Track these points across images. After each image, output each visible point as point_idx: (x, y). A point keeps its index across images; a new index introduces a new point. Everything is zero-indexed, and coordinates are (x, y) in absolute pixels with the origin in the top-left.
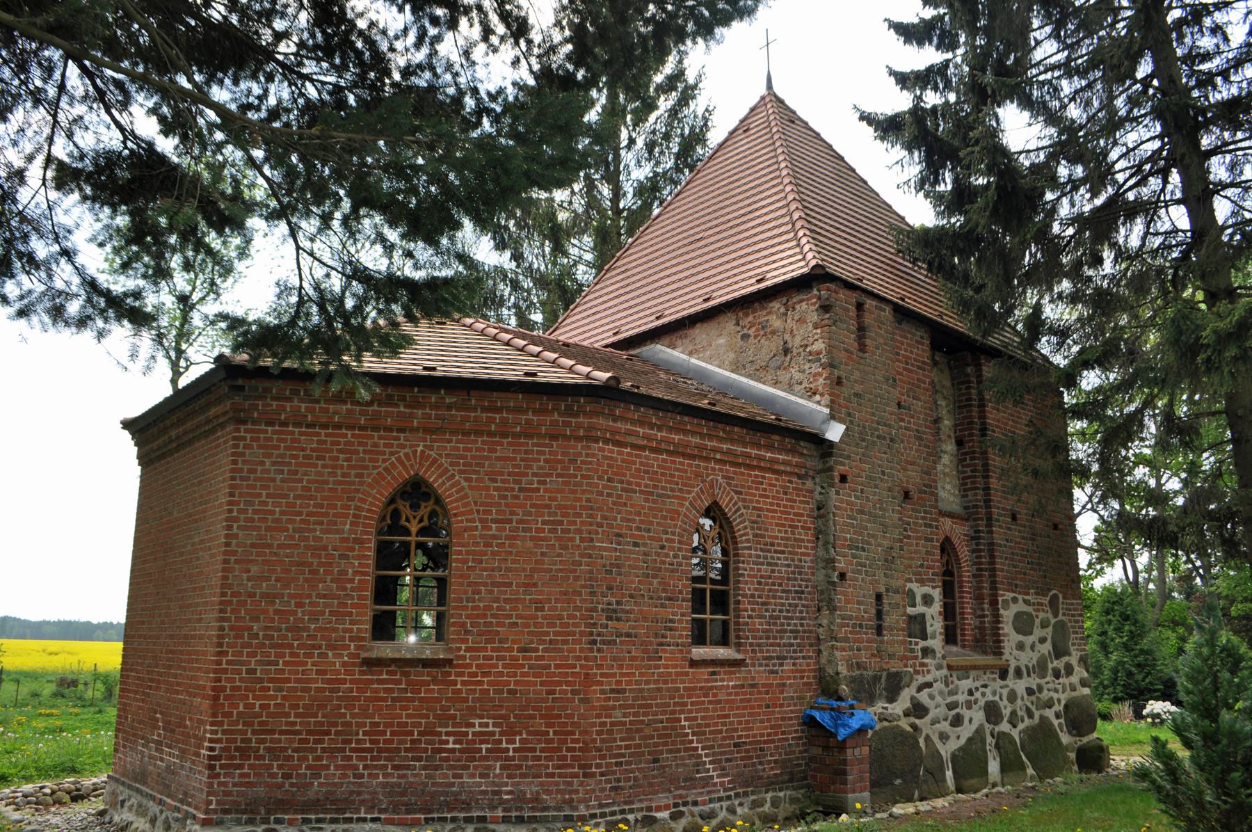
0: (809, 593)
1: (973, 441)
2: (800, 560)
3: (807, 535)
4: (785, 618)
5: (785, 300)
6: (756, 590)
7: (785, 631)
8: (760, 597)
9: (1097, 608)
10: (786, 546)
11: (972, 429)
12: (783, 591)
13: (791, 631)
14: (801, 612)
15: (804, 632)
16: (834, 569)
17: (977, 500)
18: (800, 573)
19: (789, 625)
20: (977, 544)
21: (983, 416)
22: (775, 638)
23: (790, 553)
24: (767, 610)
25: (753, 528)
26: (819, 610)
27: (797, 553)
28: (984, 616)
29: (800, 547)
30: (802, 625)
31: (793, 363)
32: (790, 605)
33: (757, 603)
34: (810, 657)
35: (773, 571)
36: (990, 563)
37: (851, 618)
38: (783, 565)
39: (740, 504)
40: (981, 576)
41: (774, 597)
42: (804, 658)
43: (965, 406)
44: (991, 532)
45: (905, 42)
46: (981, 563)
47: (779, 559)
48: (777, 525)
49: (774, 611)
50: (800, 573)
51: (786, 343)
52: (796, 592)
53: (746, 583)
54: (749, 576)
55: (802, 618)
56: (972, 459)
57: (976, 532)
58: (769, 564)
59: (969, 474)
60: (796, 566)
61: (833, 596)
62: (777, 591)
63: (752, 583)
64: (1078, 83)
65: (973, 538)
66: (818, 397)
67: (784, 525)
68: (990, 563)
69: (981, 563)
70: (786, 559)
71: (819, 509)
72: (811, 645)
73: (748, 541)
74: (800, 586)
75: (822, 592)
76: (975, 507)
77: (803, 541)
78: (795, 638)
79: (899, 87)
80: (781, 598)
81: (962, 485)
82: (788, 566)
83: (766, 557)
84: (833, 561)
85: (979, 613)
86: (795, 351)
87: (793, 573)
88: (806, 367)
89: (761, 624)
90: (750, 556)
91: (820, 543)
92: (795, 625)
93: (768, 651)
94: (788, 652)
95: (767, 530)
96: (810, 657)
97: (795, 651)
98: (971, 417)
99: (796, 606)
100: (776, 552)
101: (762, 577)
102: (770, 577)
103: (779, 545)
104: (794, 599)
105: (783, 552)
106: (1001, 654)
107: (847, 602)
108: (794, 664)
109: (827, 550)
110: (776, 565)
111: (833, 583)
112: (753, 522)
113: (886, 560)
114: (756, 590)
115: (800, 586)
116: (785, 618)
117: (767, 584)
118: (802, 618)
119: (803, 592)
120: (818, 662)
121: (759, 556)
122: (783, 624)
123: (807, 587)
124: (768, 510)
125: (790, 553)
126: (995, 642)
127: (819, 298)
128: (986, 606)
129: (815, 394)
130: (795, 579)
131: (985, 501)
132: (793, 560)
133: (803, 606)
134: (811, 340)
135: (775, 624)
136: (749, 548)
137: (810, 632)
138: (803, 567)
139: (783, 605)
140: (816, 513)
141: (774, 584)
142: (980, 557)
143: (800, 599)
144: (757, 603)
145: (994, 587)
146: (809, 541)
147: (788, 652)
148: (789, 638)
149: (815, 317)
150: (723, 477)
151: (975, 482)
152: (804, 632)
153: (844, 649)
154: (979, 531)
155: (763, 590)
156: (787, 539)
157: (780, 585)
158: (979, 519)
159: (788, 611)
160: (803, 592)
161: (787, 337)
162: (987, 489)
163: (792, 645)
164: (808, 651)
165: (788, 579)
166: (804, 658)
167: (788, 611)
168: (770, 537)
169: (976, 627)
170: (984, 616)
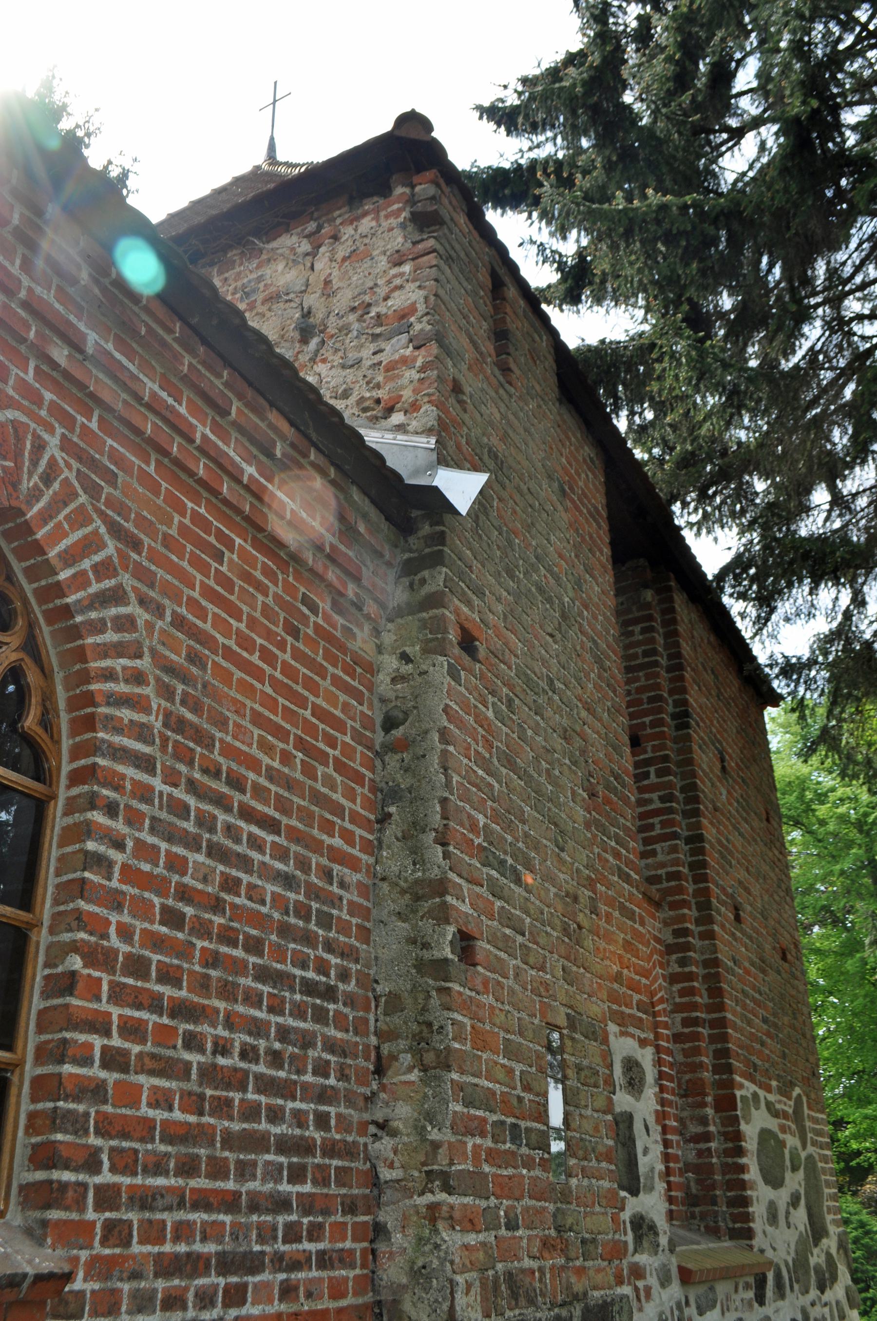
0: (350, 1001)
1: (661, 735)
2: (328, 875)
3: (351, 795)
4: (266, 1085)
5: (312, 226)
6: (157, 942)
7: (259, 1142)
8: (168, 976)
9: (147, 1215)
10: (283, 806)
11: (660, 710)
12: (263, 974)
13: (284, 1146)
14: (322, 1070)
15: (330, 1150)
16: (443, 915)
17: (676, 862)
18: (325, 921)
19: (275, 1116)
20: (683, 962)
21: (679, 688)
22: (218, 1170)
23: (295, 836)
24: (192, 1042)
25: (167, 693)
26: (380, 1070)
27: (316, 846)
28: (706, 1137)
29: (328, 827)
30: (322, 1121)
31: (326, 352)
32: (284, 1034)
33: (155, 1004)
34: (345, 1259)
35: (231, 885)
36: (710, 1009)
37: (487, 1101)
38: (265, 871)
39: (126, 580)
40: (696, 1037)
41: (228, 992)
42: (324, 1260)
43: (641, 667)
44: (709, 935)
45: (509, 133)
46: (694, 1007)
47: (256, 844)
48: (258, 720)
49: (221, 1048)
50: (325, 921)
51: (307, 314)
52: (309, 988)
53: (115, 901)
54: (129, 874)
55: (324, 1096)
56: (660, 773)
57: (677, 933)
58: (216, 852)
59: (657, 805)
60: (313, 892)
61: (438, 1016)
62: (239, 967)
63: (142, 910)
64: (677, 392)
65: (670, 949)
66: (397, 418)
67: (281, 733)
68: (710, 1009)
69: (694, 1007)
70: (282, 854)
71: (389, 724)
72: (351, 1208)
73: (142, 733)
74: (322, 968)
75: (394, 1003)
76: (675, 876)
77: (339, 810)
78: (297, 1175)
79: (533, 71)
80: (253, 999)
81: (641, 829)
82: (288, 881)
83: (206, 822)
84: (441, 887)
85: (694, 1129)
86: (333, 324)
87: (303, 912)
88: (366, 353)
89: (161, 1100)
90: (145, 793)
91: (392, 831)
92: (299, 1119)
93: (182, 1232)
94: (266, 1234)
95: (222, 723)
96: (345, 1259)
97: (292, 1234)
98: (657, 686)
99: (306, 1041)
100: (247, 814)
101: (185, 894)
102: (217, 906)
103: (259, 792)
104: (299, 1012)
105: (273, 826)
106: (749, 1234)
107: (481, 1041)
108: (288, 1291)
109: (417, 856)
110: (245, 863)
111: (440, 968)
112: (171, 669)
113: (565, 930)
114: (157, 942)
115: (322, 968)
116: (266, 1085)
117: (202, 930)
118: (324, 1096)
119: (330, 994)
120: (370, 1282)
121: (181, 810)
122: (251, 1112)
123: (344, 976)
124: (228, 653)
125: (295, 836)
126: (731, 1203)
127: (411, 201)
128: (710, 1111)
129: (390, 410)
130: (308, 939)
131: (692, 866)
132: (304, 865)
133: (331, 1046)
134: (382, 291)
135: (222, 1107)
136: (147, 764)
137: (349, 1151)
138: (335, 901)
139: (257, 1028)
140: (379, 738)
141: (228, 937)
142: (691, 992)
143: (320, 1016)
144: (155, 1004)
145: (724, 1068)
146: (355, 818)
147: (266, 1234)
148: (274, 1173)
149: (398, 241)
150: (66, 445)
151: (671, 823)
152: (330, 1150)
153: (471, 1226)
154: (685, 932)
155: (185, 951)
156: (290, 784)
157: (254, 946)
158: (684, 904)
159: (276, 1058)
160: (330, 994)
161: (312, 300)
162: (696, 840)
163: (282, 1204)
164: (339, 1230)
165: (284, 930)
166: (324, 1260)
167: (276, 1058)
168: (228, 751)
169: (688, 1167)
170: (706, 1137)
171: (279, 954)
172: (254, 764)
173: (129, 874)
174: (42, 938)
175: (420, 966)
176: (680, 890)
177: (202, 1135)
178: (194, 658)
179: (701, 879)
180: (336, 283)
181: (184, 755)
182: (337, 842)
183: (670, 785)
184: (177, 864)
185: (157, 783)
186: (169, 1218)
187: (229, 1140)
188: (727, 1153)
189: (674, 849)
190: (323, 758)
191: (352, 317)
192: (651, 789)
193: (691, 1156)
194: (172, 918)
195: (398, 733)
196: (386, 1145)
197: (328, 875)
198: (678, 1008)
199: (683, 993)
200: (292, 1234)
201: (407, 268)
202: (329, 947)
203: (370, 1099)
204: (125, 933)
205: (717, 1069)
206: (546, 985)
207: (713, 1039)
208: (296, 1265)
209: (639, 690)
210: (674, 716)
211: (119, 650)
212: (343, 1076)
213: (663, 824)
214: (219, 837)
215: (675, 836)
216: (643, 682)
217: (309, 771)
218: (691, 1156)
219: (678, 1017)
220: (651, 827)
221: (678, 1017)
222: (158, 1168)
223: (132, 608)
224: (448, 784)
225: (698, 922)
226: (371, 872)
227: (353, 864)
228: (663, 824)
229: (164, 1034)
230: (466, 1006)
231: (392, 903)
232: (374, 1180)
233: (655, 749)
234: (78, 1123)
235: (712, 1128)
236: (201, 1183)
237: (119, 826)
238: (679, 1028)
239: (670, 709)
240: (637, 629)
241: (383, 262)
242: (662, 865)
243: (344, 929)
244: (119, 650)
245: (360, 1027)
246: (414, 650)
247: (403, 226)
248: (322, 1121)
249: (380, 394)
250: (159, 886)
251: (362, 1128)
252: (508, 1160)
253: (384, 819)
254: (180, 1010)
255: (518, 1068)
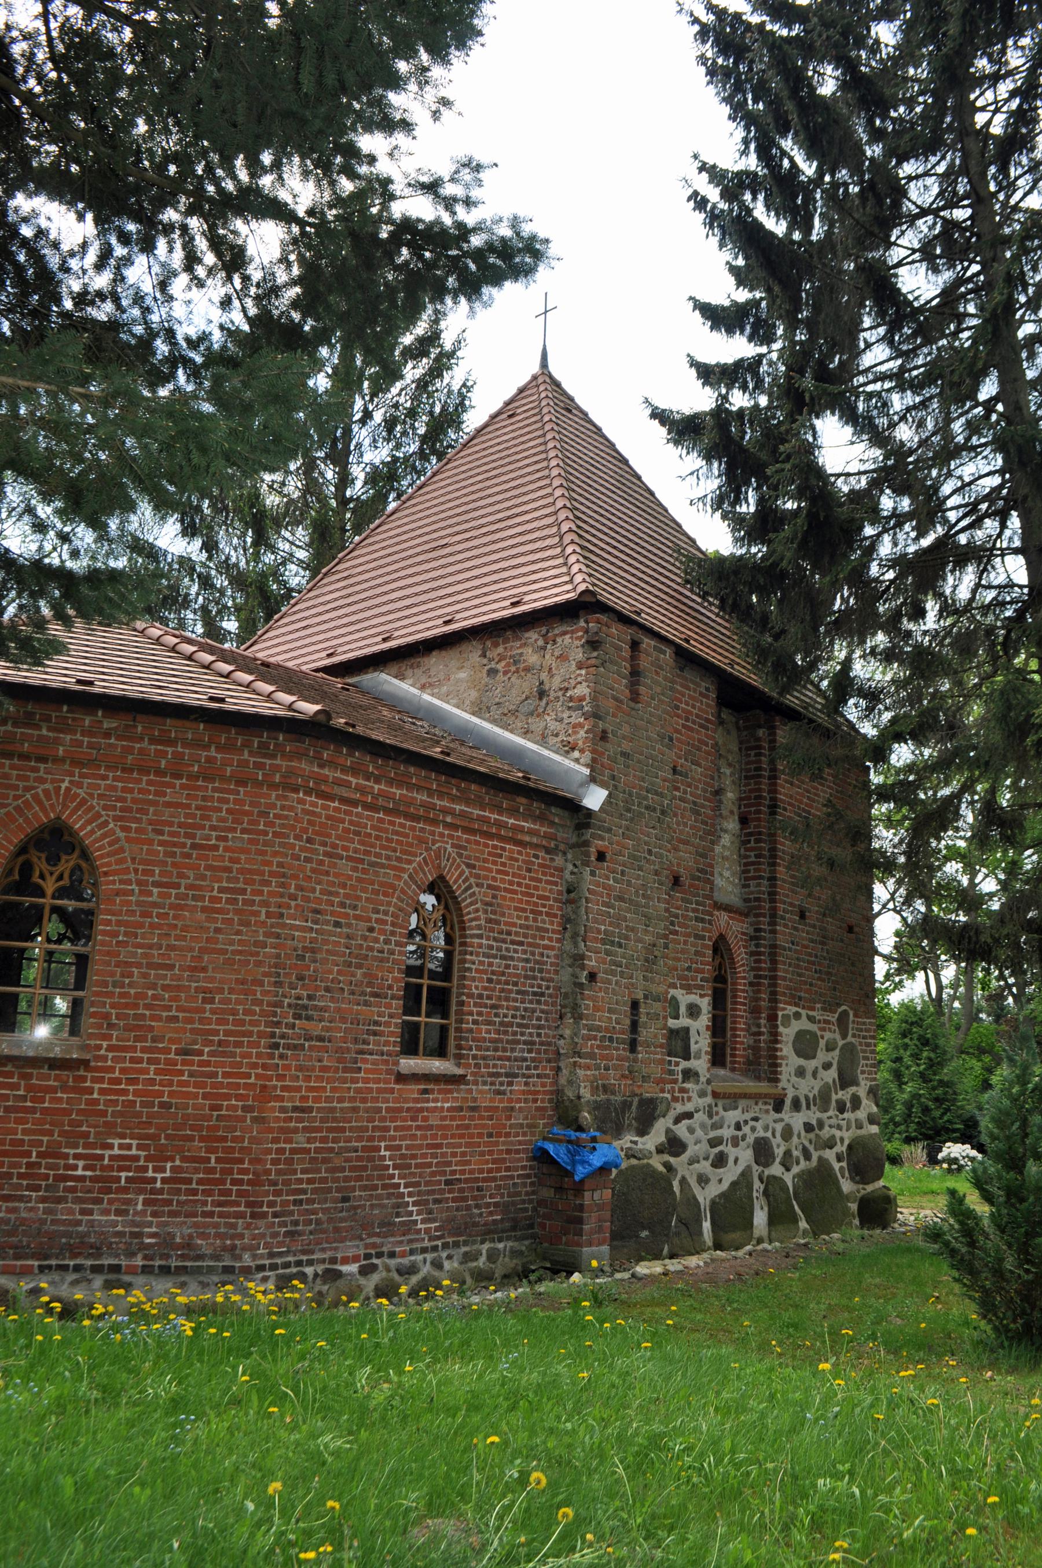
0: (550, 996)
1: (759, 820)
4: (519, 1025)
5: (544, 630)
6: (485, 988)
7: (518, 1042)
8: (489, 997)
10: (525, 936)
12: (518, 992)
13: (525, 1043)
14: (539, 1019)
15: (542, 1043)
16: (583, 967)
18: (541, 971)
19: (523, 1034)
20: (757, 946)
22: (505, 1050)
23: (530, 945)
24: (497, 1015)
26: (561, 1018)
27: (538, 946)
28: (760, 1034)
29: (542, 938)
30: (539, 1035)
32: (525, 1010)
34: (547, 1076)
35: (507, 967)
36: (770, 970)
37: (599, 1029)
38: (520, 960)
39: (472, 880)
40: (759, 984)
41: (507, 999)
42: (539, 1076)
44: (774, 932)
46: (760, 969)
48: (516, 909)
49: (505, 1016)
50: (541, 971)
51: (542, 683)
52: (535, 994)
53: (473, 979)
54: (477, 971)
55: (539, 1027)
56: (757, 841)
57: (757, 930)
59: (753, 859)
60: (537, 962)
61: (579, 1001)
62: (510, 991)
63: (481, 980)
66: (576, 754)
67: (524, 910)
68: (770, 970)
69: (760, 969)
70: (525, 952)
71: (569, 891)
72: (549, 1061)
73: (479, 927)
75: (566, 996)
77: (547, 930)
78: (530, 1051)
79: (700, 382)
80: (515, 1000)
82: (527, 961)
83: (499, 949)
85: (754, 1029)
86: (552, 694)
87: (532, 970)
89: (488, 1032)
90: (480, 946)
91: (568, 935)
92: (531, 1035)
93: (495, 1066)
95: (503, 915)
96: (547, 1076)
97: (528, 1068)
98: (760, 790)
99: (534, 1011)
100: (513, 942)
101: (493, 973)
102: (503, 974)
103: (517, 934)
104: (531, 1002)
105: (521, 944)
106: (777, 1080)
107: (597, 1009)
108: (526, 1084)
110: (512, 959)
111: (581, 985)
112: (487, 904)
113: (647, 960)
114: (485, 988)
115: (540, 986)
116: (519, 1025)
117: (499, 982)
118: (539, 1027)
119: (542, 994)
120: (556, 1083)
121: (491, 947)
122: (515, 1034)
123: (548, 988)
124: (506, 890)
125: (530, 945)
126: (770, 1065)
127: (587, 631)
128: (763, 1022)
129: (573, 749)
130: (534, 978)
132: (533, 954)
133: (542, 1011)
134: (573, 682)
135: (506, 1033)
136: (480, 936)
137: (549, 1044)
138: (545, 963)
139: (517, 1009)
140: (565, 897)
141: (507, 983)
143: (539, 1002)
144: (486, 1006)
147: (520, 1068)
148: (523, 1051)
150: (453, 846)
152: (542, 1043)
153: (588, 1067)
155: (494, 990)
156: (528, 927)
157: (515, 984)
159: (523, 1017)
160: (542, 994)
161: (544, 676)
163: (525, 1059)
165: (526, 977)
166: (539, 1076)
167: (523, 1017)
168: (506, 924)
170: (760, 1034)
171: (524, 985)
172: (514, 925)
173: (477, 971)
174: (455, 990)
175: (575, 984)
176: (759, 907)
177: (500, 1041)
178: (494, 897)
179: (773, 901)
180: (554, 671)
181: (492, 930)
182: (546, 942)
183: (761, 849)
184: (490, 964)
185: (484, 942)
186: (491, 1063)
187: (508, 1042)
188: (771, 1042)
189: (759, 885)
190: (540, 913)
191: (560, 693)
192: (752, 849)
193: (751, 1042)
194: (490, 981)
195: (572, 895)
196: (562, 1042)
197: (542, 955)
198: (753, 969)
199: (756, 961)
200: (528, 1068)
201: (583, 672)
202: (542, 979)
203: (557, 1027)
204: (477, 988)
205: (770, 1001)
206: (633, 985)
207: (770, 985)
208: (529, 1077)
209: (751, 791)
210: (769, 807)
211: (471, 904)
212: (547, 1020)
213: (755, 870)
214: (504, 953)
215: (760, 877)
216: (752, 786)
217: (535, 920)
218: (751, 1042)
219: (752, 973)
220: (749, 871)
221: (752, 973)
222: (488, 1050)
223: (475, 889)
224: (588, 919)
225: (769, 924)
226: (560, 949)
227: (552, 948)
228: (755, 870)
229: (489, 1013)
230: (589, 998)
231: (568, 961)
232: (559, 1054)
233: (755, 827)
234: (467, 1039)
235: (763, 1029)
236: (500, 1053)
237: (474, 958)
238: (752, 979)
239: (767, 802)
240: (753, 753)
241: (573, 666)
242: (752, 893)
243: (548, 972)
244: (471, 904)
245: (554, 1004)
246: (578, 863)
247: (583, 646)
248: (539, 1035)
249: (570, 739)
250: (485, 972)
251: (554, 1037)
252: (606, 1048)
253: (565, 929)
254: (493, 1007)
255: (614, 1017)
